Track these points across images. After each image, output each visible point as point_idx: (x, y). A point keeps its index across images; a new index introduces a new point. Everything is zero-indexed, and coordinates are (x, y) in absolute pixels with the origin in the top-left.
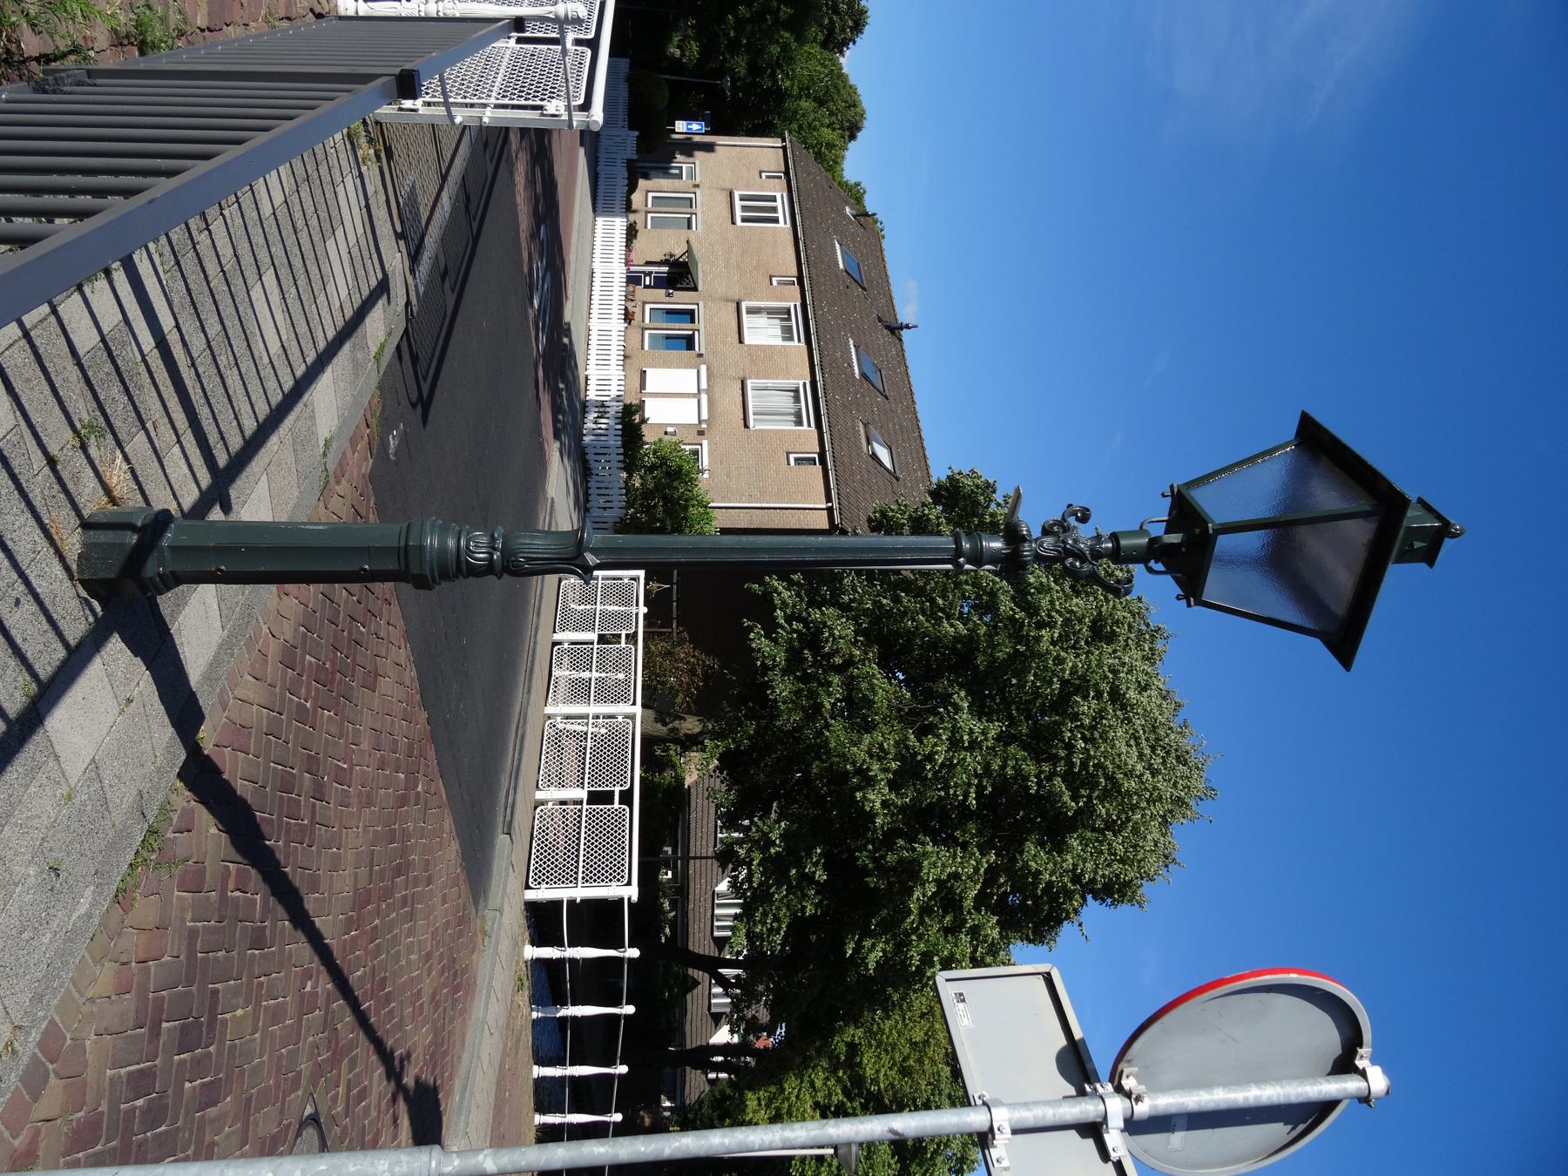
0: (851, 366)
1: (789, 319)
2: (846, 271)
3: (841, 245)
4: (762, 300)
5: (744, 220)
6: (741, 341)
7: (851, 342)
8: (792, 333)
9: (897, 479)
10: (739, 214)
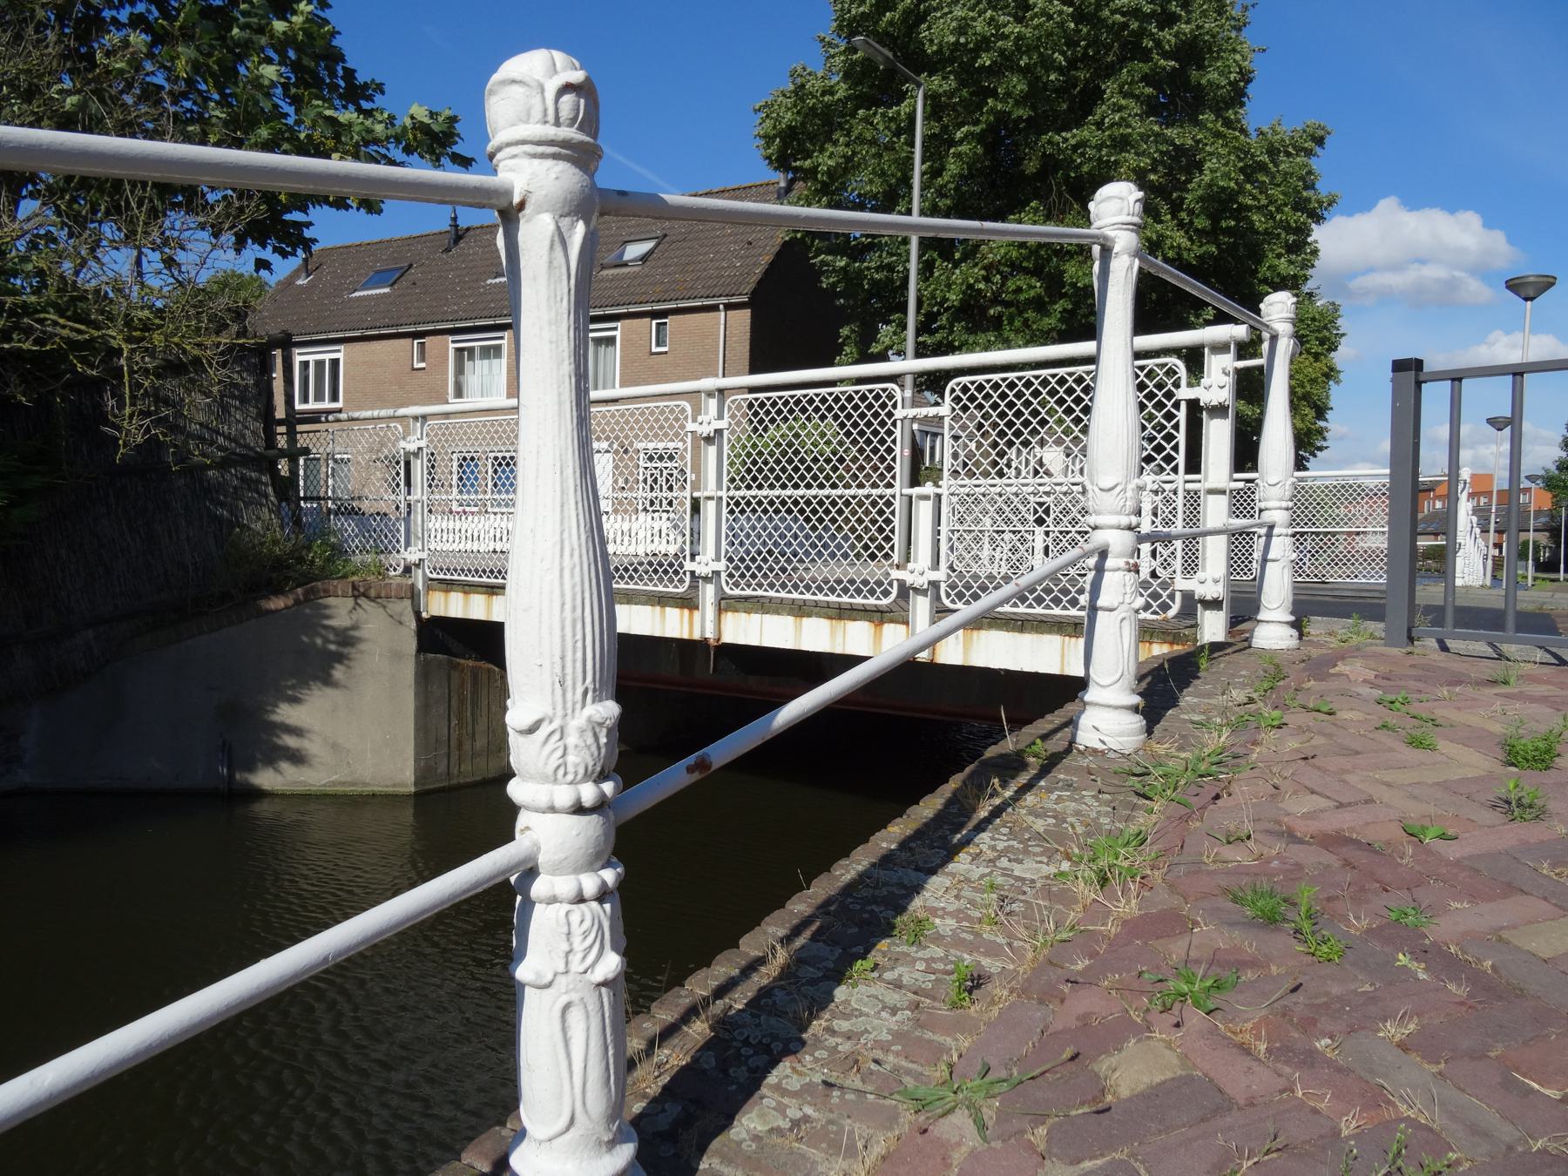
1: (471, 350)
2: (392, 285)
3: (355, 291)
4: (446, 380)
5: (335, 398)
7: (489, 282)
8: (489, 347)
9: (665, 236)
10: (326, 405)
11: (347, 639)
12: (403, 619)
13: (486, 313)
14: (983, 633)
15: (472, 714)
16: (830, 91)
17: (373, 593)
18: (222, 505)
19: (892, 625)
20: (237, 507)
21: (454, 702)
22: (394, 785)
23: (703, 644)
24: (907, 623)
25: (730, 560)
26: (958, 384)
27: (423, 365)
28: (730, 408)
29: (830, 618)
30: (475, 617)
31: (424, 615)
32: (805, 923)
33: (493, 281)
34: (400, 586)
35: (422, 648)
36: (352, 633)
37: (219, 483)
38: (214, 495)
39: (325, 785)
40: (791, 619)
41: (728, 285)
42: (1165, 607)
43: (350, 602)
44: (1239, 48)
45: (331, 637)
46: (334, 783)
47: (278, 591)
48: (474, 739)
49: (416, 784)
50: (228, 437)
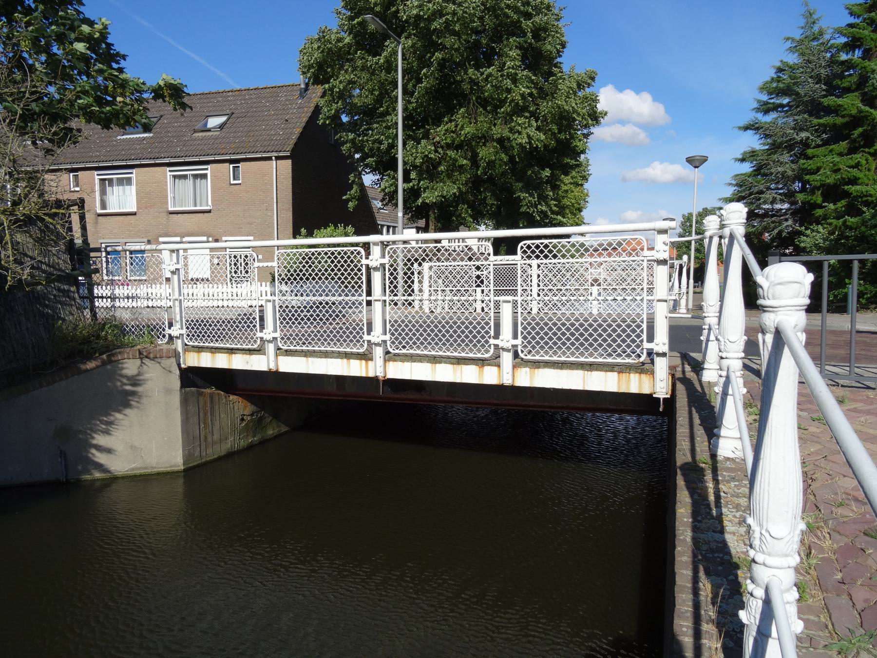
0: (144, 139)
1: (110, 181)
6: (134, 214)
7: (119, 138)
11: (135, 381)
12: (172, 369)
13: (119, 157)
14: (541, 370)
15: (211, 421)
16: (339, 40)
17: (152, 356)
18: (47, 306)
19: (489, 367)
20: (57, 308)
21: (201, 415)
22: (171, 467)
23: (375, 379)
24: (499, 366)
25: (393, 334)
26: (525, 244)
27: (77, 189)
28: (389, 252)
29: (453, 364)
30: (220, 367)
31: (183, 366)
32: (695, 580)
33: (122, 137)
34: (168, 350)
35: (184, 385)
36: (137, 378)
37: (44, 293)
38: (42, 300)
39: (127, 471)
40: (429, 365)
41: (277, 145)
42: (639, 356)
43: (138, 362)
44: (559, 31)
45: (125, 381)
46: (133, 469)
47: (89, 357)
48: (213, 435)
49: (184, 464)
50: (48, 265)
